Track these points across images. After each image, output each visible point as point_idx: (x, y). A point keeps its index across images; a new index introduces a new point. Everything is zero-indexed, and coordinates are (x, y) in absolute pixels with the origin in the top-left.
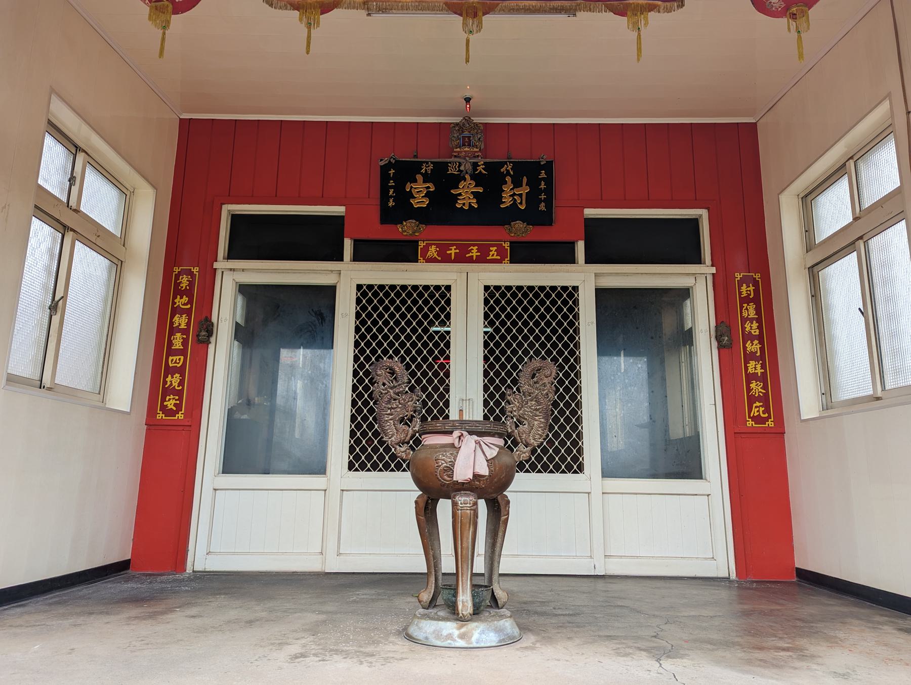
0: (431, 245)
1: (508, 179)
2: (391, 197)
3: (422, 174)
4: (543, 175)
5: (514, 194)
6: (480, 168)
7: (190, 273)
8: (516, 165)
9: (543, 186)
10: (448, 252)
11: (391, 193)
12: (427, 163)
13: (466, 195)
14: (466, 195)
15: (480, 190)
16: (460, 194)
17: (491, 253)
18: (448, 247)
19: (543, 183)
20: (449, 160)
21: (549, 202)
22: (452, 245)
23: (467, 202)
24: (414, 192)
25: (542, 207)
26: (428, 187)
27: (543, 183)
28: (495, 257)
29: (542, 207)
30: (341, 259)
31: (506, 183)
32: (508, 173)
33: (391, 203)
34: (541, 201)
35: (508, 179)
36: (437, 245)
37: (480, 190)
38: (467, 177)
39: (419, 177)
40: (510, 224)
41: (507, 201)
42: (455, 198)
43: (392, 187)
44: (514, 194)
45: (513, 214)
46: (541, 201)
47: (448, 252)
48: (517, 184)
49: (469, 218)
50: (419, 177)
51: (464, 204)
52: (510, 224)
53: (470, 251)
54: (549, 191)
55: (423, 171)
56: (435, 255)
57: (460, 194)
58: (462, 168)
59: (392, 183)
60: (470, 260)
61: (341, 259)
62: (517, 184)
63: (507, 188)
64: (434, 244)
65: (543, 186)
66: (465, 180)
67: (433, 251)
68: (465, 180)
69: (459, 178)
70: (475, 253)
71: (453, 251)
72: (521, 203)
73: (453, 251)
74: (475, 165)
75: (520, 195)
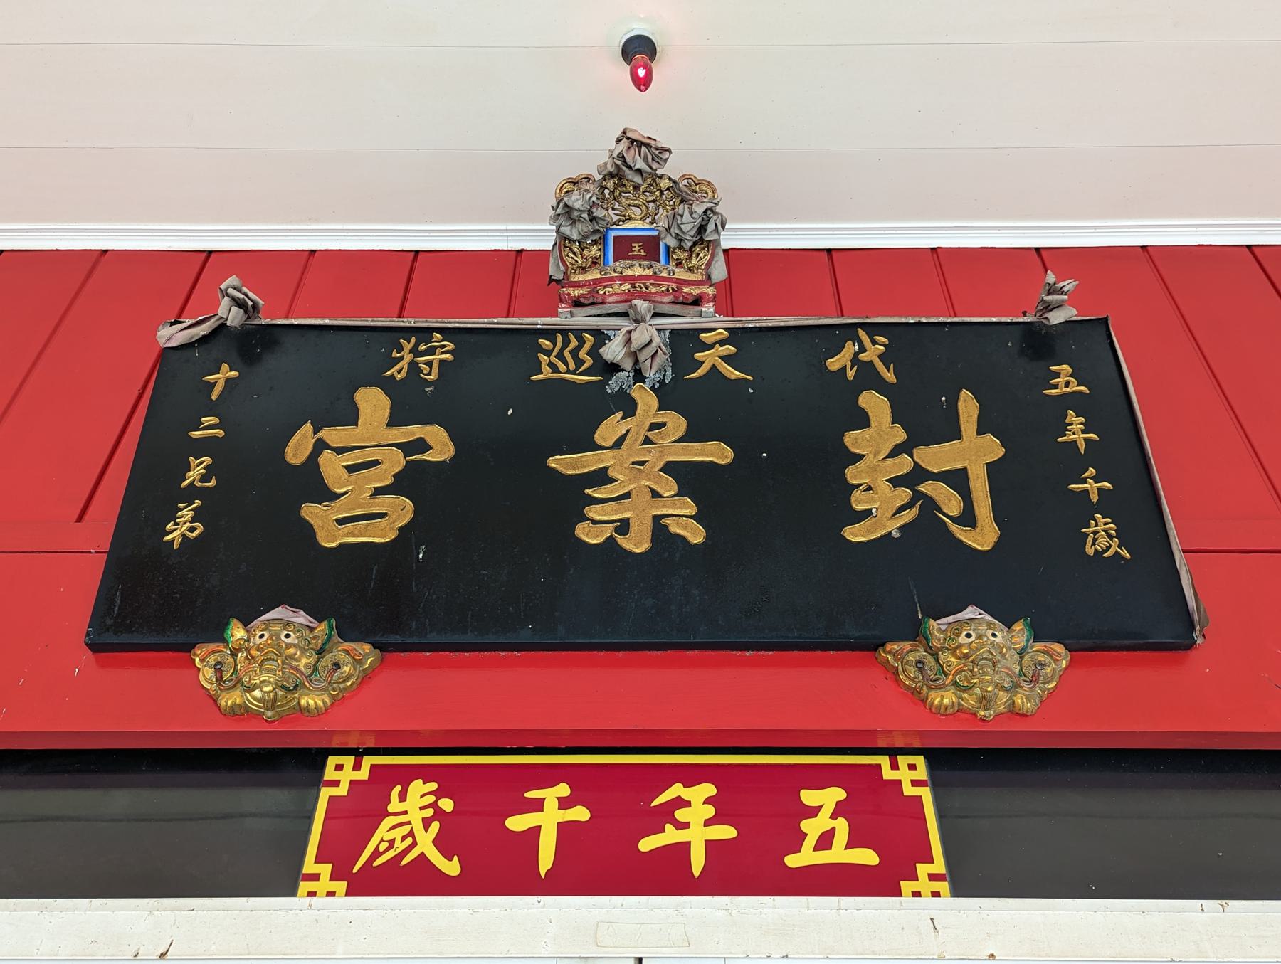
0: (405, 776)
1: (874, 403)
2: (192, 493)
3: (388, 386)
4: (1065, 381)
5: (917, 475)
6: (708, 359)
7: (429, 374)
8: (902, 339)
9: (1077, 432)
10: (517, 823)
11: (195, 474)
12: (424, 333)
13: (637, 482)
14: (637, 482)
15: (718, 453)
16: (601, 477)
17: (812, 828)
18: (515, 789)
19: (1075, 421)
20: (540, 322)
21: (1139, 508)
22: (548, 776)
23: (640, 517)
24: (332, 467)
25: (1102, 536)
26: (421, 445)
27: (1075, 421)
28: (839, 854)
29: (1102, 536)
30: (956, 435)
31: (862, 420)
32: (867, 376)
33: (183, 527)
34: (1084, 509)
35: (874, 403)
36: (447, 781)
37: (718, 453)
38: (646, 399)
39: (373, 403)
40: (915, 632)
41: (879, 509)
42: (574, 495)
43: (202, 447)
44: (917, 475)
45: (925, 577)
46: (1084, 509)
47: (517, 823)
48: (925, 422)
49: (647, 605)
50: (373, 403)
51: (623, 527)
52: (915, 632)
53: (667, 814)
54: (1122, 449)
55: (399, 372)
56: (425, 844)
57: (601, 477)
58: (613, 351)
59: (209, 428)
60: (668, 875)
61: (956, 435)
62: (925, 422)
63: (876, 438)
64: (426, 773)
65: (1077, 432)
66: (629, 408)
67: (412, 820)
68: (629, 408)
69: (597, 400)
70: (696, 823)
71: (548, 817)
72: (968, 518)
73: (548, 817)
74: (684, 344)
75: (958, 480)
